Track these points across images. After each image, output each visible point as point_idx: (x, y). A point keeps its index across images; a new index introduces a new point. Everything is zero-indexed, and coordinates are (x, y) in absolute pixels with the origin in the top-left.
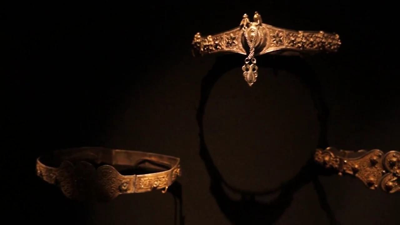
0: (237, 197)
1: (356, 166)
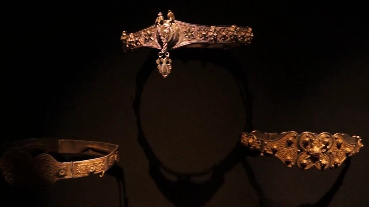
0: (172, 178)
1: (275, 147)
